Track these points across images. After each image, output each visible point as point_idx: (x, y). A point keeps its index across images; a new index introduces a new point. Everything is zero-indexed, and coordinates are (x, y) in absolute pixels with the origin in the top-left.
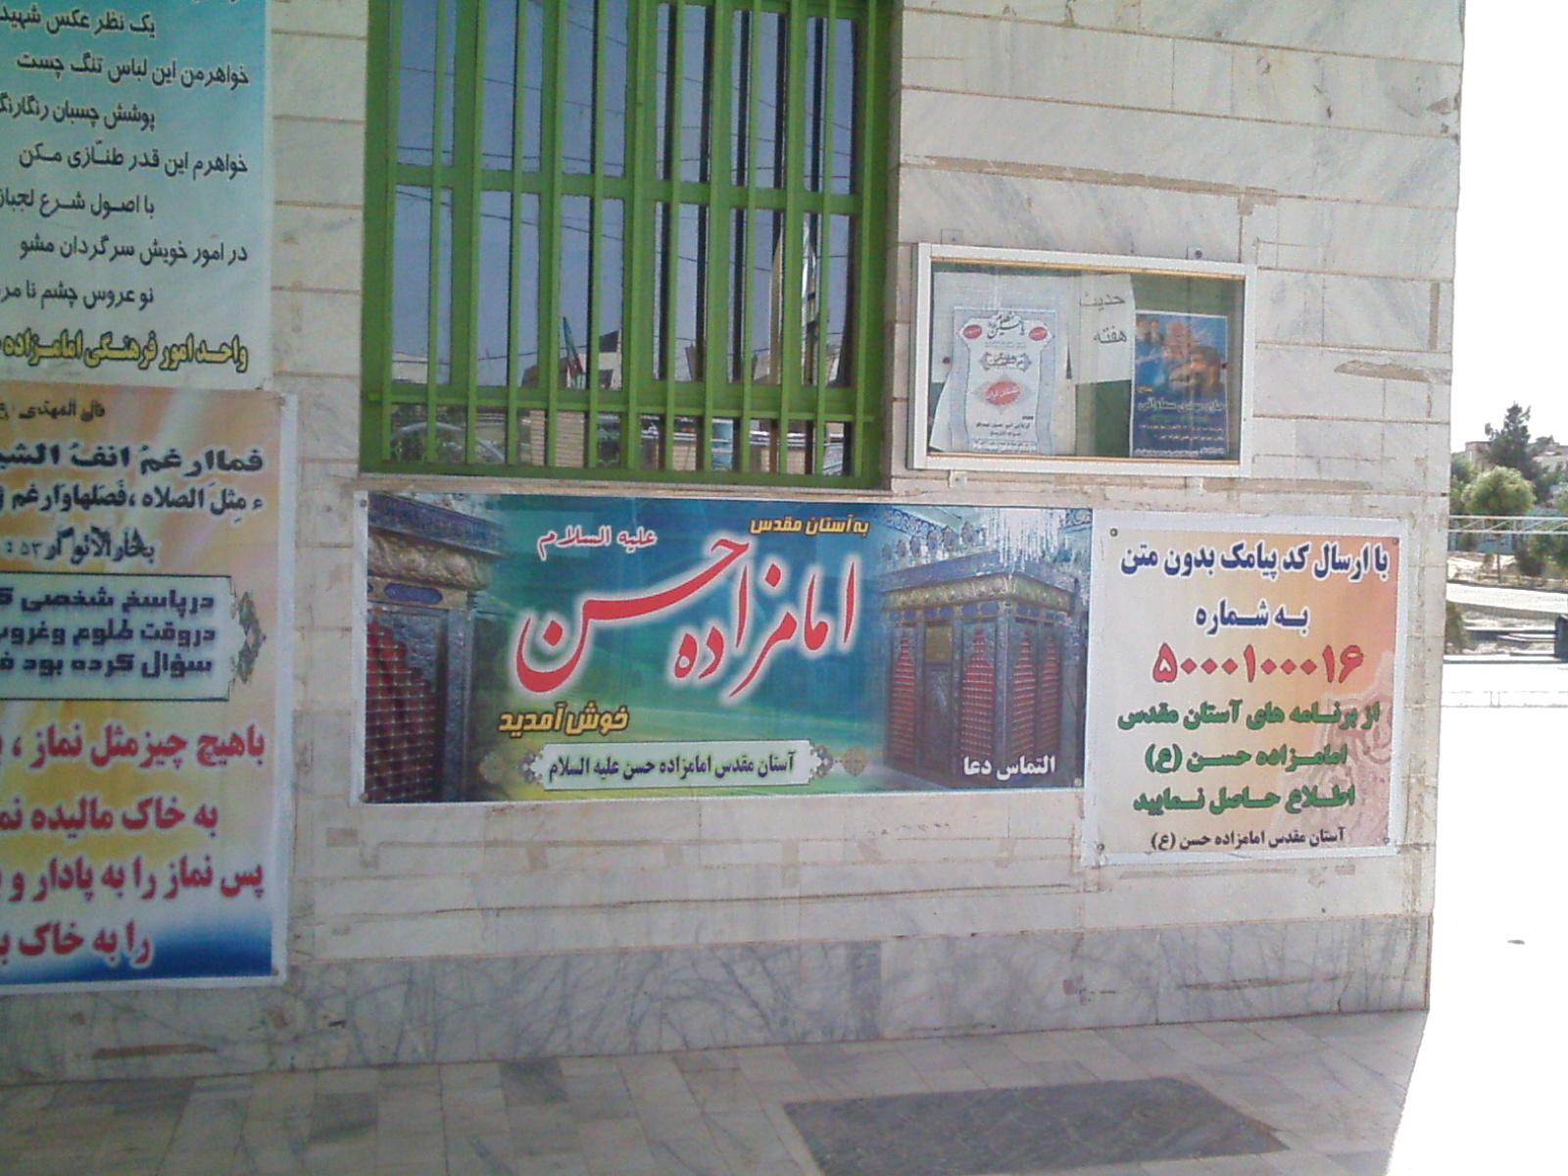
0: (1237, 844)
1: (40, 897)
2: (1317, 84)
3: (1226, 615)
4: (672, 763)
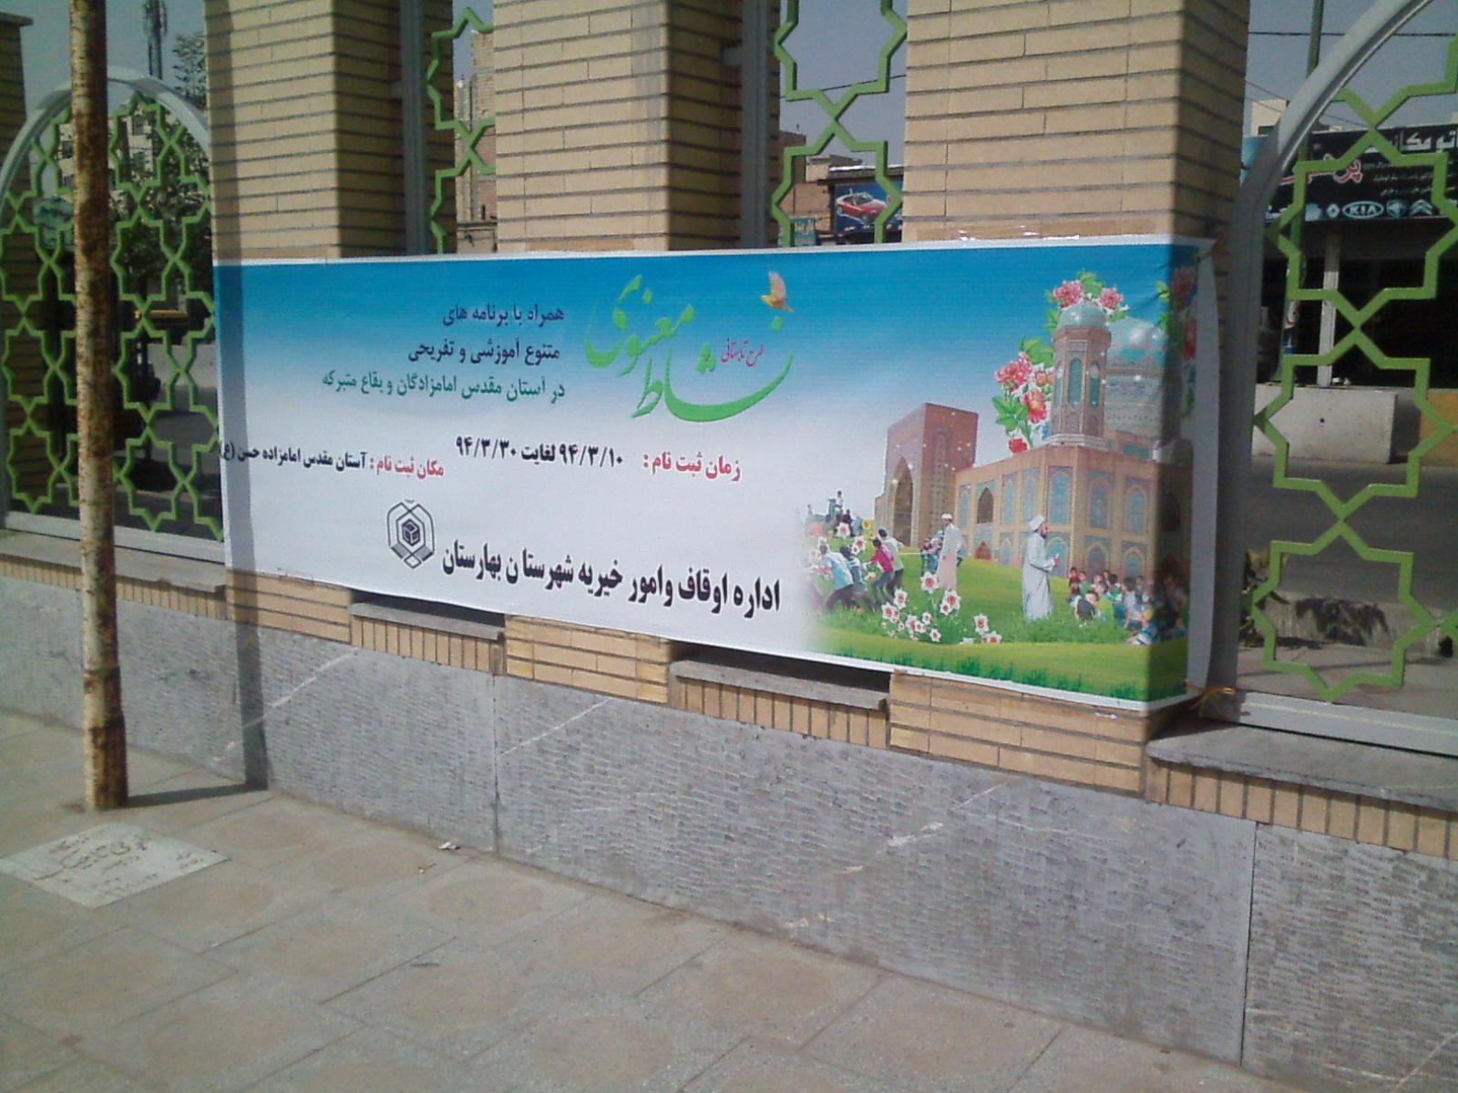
0: (279, 460)
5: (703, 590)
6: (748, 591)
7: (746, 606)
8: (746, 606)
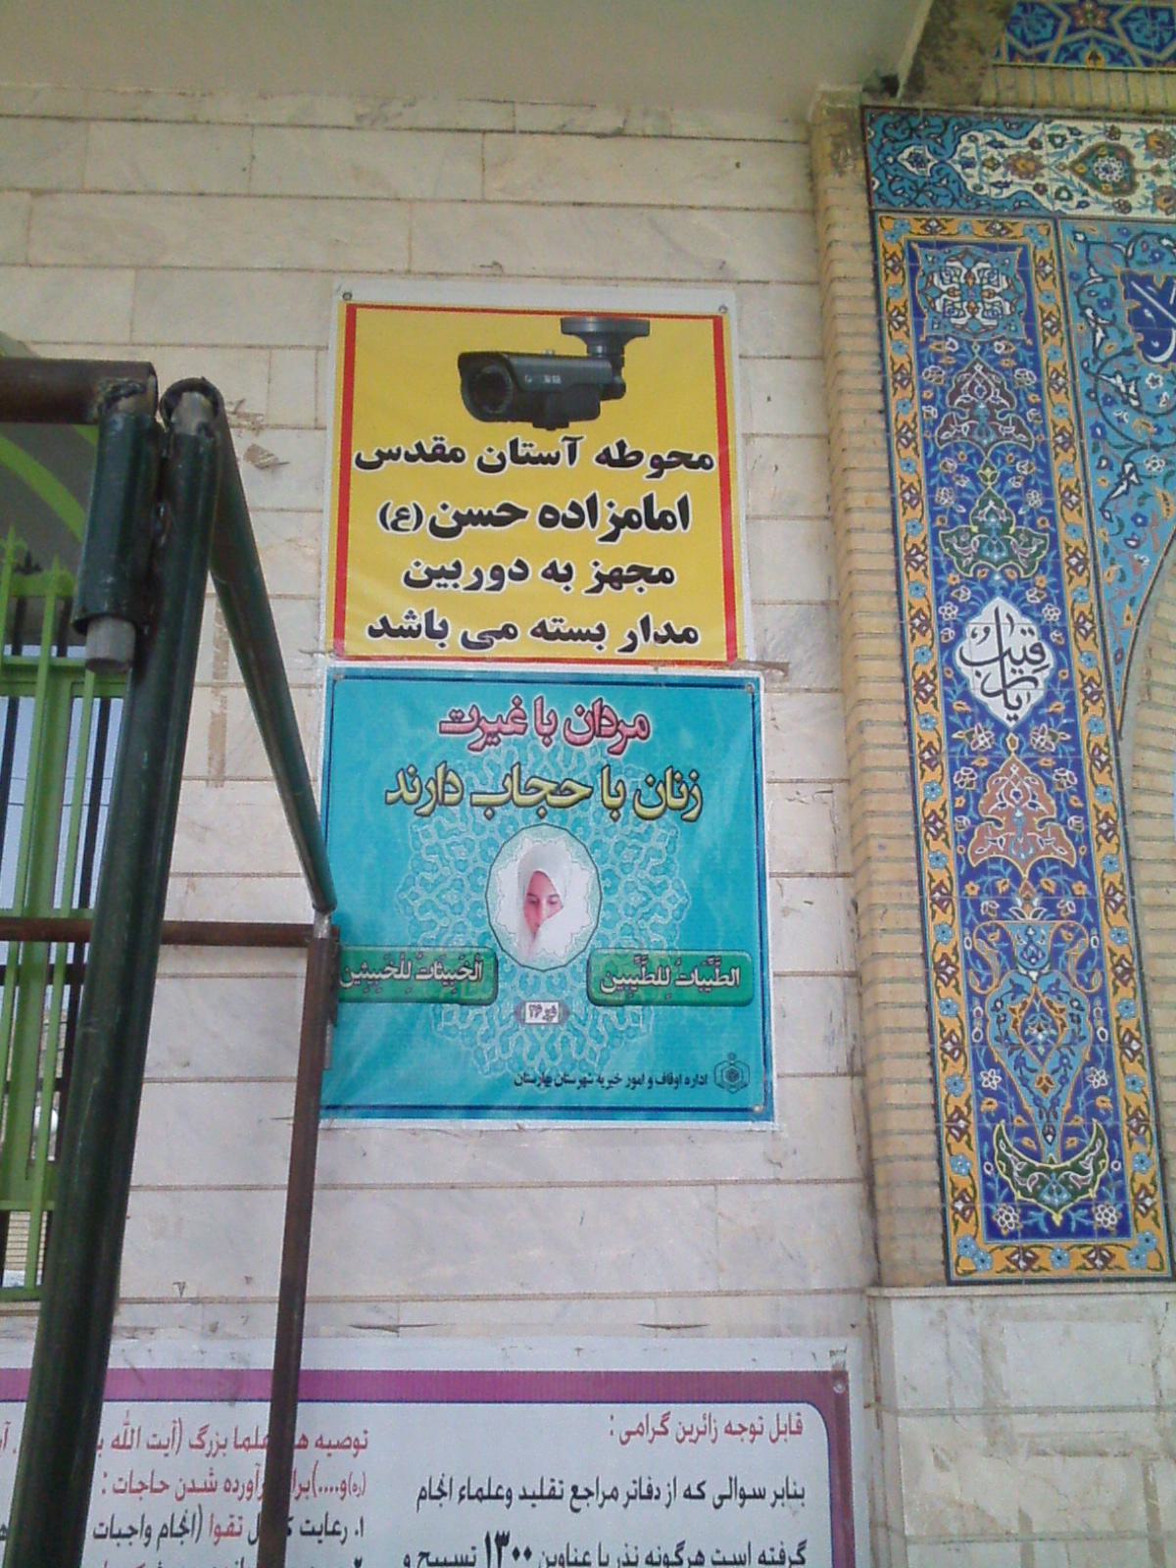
3: (656, 516)
4: (574, 507)
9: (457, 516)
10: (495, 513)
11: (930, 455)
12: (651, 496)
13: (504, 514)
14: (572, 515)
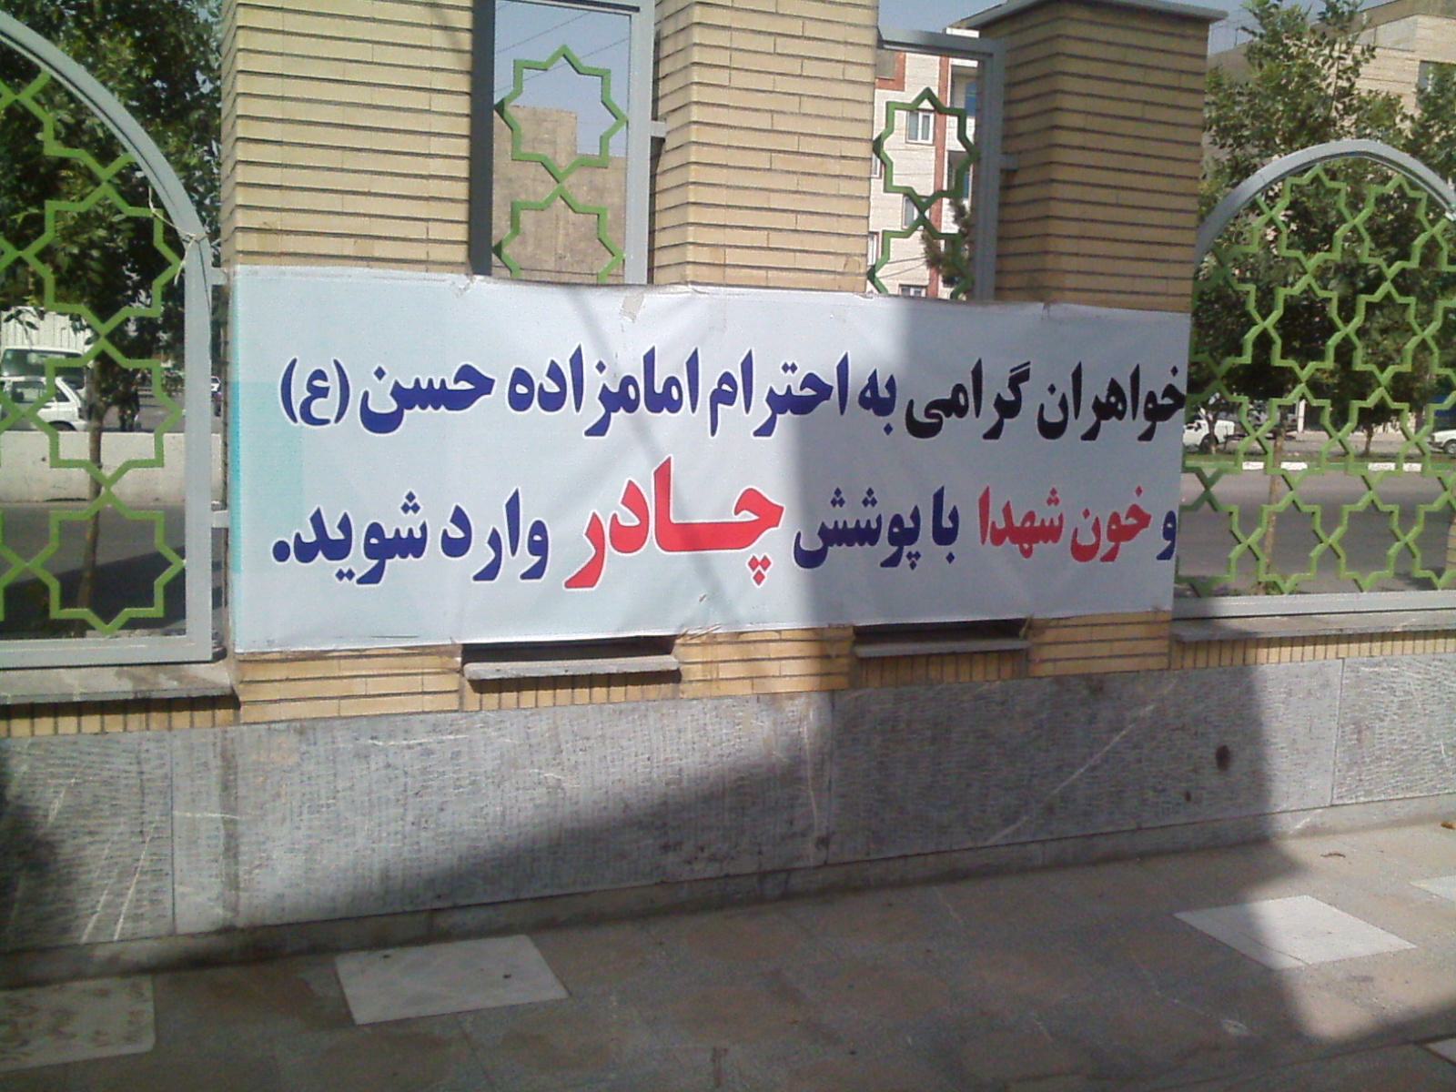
0: (594, 410)
1: (587, 577)
2: (34, 332)
3: (659, 389)
4: (555, 372)
5: (947, 523)
6: (487, 520)
7: (480, 554)
8: (480, 554)
9: (398, 392)
10: (451, 386)
11: (121, 227)
12: (318, 512)
13: (465, 385)
14: (552, 388)
